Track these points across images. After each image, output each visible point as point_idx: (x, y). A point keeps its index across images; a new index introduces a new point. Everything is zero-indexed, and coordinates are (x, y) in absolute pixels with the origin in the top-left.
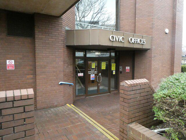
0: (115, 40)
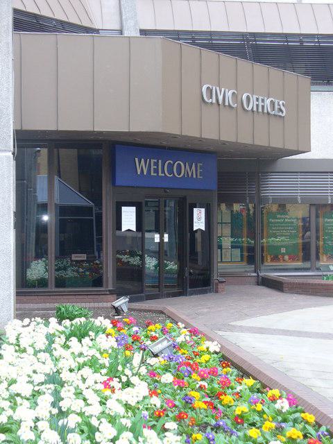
0: (214, 101)
